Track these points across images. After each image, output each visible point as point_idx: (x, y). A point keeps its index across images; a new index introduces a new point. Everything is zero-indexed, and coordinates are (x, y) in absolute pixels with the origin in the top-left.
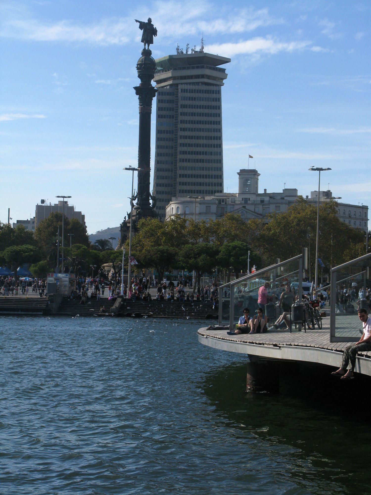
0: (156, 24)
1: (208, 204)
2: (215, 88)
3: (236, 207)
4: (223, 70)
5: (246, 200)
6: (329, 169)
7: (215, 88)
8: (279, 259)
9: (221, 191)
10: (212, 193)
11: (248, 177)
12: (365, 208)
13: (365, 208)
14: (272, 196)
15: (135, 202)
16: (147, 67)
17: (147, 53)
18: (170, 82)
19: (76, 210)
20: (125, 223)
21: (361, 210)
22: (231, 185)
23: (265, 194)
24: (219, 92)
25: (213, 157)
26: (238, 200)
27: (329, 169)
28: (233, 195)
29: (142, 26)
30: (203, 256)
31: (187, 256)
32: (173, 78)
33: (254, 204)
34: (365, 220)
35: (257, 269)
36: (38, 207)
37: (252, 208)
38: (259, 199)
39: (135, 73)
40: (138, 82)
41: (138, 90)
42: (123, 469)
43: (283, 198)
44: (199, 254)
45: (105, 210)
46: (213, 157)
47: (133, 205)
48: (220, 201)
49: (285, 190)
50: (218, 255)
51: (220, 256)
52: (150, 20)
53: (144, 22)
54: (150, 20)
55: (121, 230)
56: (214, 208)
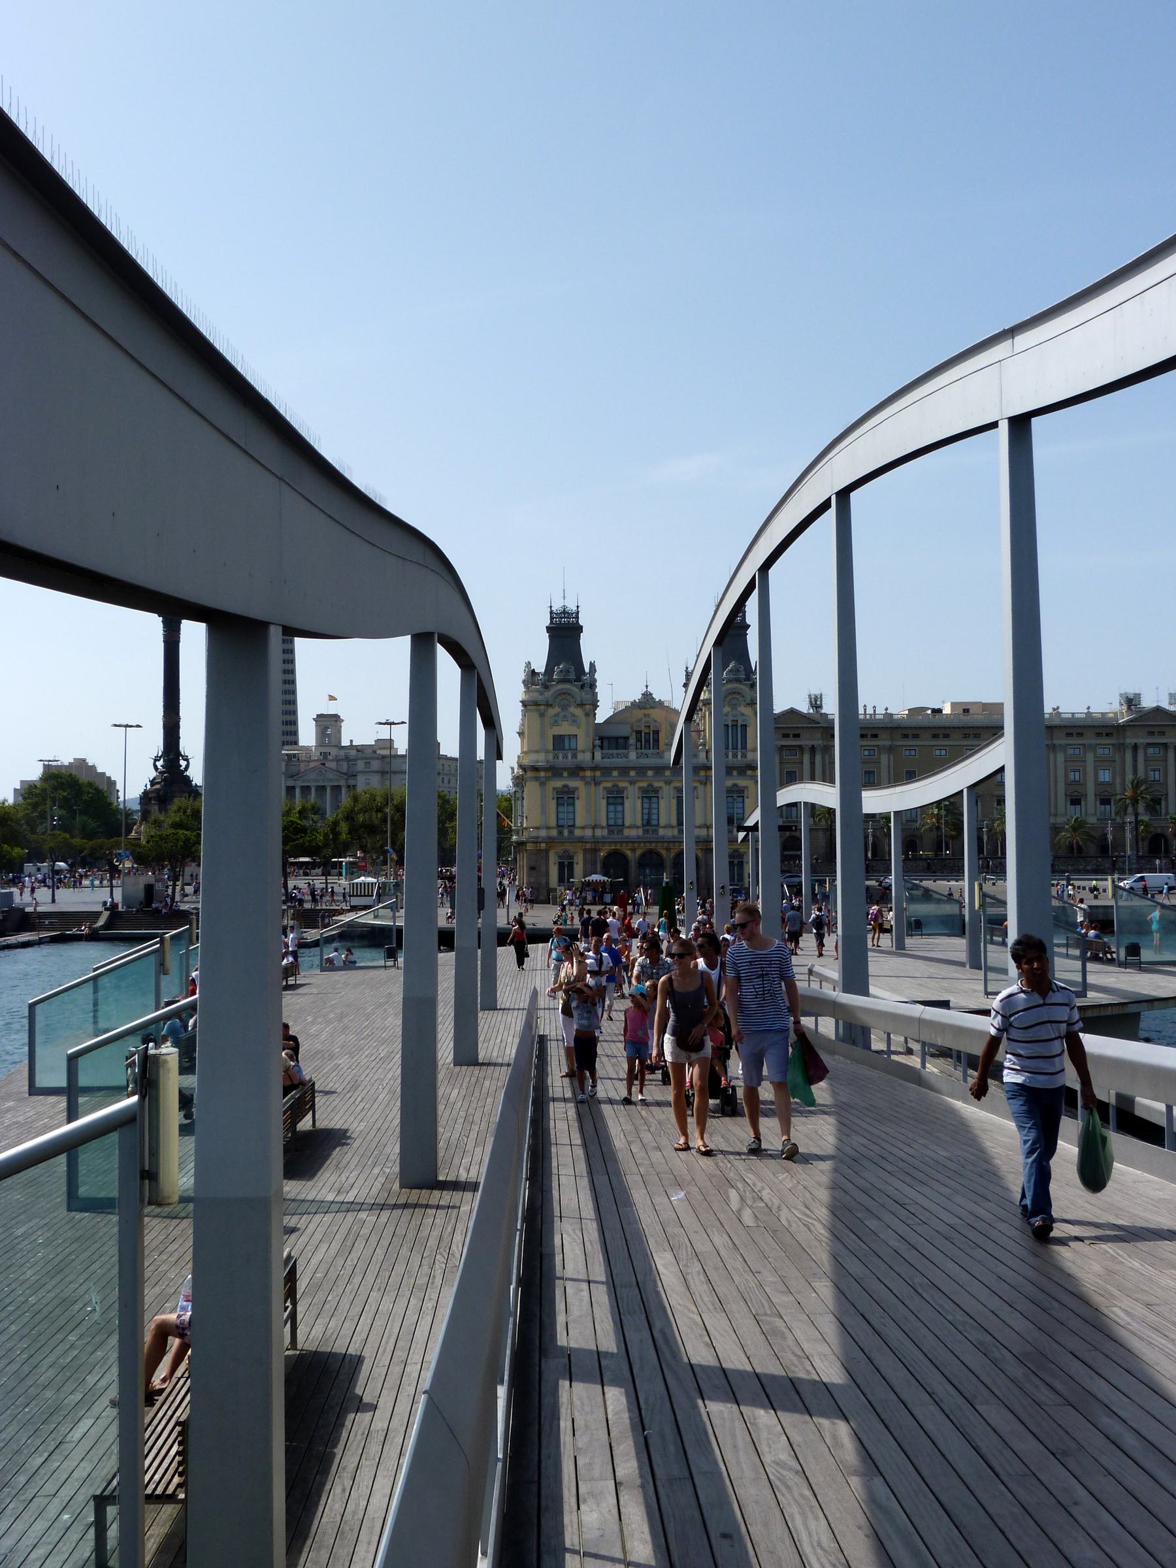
3: (312, 765)
5: (325, 755)
6: (138, 726)
8: (120, 909)
9: (296, 743)
11: (328, 724)
14: (360, 749)
15: (160, 764)
19: (99, 771)
20: (146, 793)
22: (307, 736)
23: (352, 746)
26: (315, 755)
27: (138, 726)
28: (307, 748)
33: (337, 760)
37: (333, 765)
38: (342, 753)
42: (735, 785)
43: (375, 752)
47: (156, 768)
48: (290, 757)
49: (378, 741)
55: (141, 803)
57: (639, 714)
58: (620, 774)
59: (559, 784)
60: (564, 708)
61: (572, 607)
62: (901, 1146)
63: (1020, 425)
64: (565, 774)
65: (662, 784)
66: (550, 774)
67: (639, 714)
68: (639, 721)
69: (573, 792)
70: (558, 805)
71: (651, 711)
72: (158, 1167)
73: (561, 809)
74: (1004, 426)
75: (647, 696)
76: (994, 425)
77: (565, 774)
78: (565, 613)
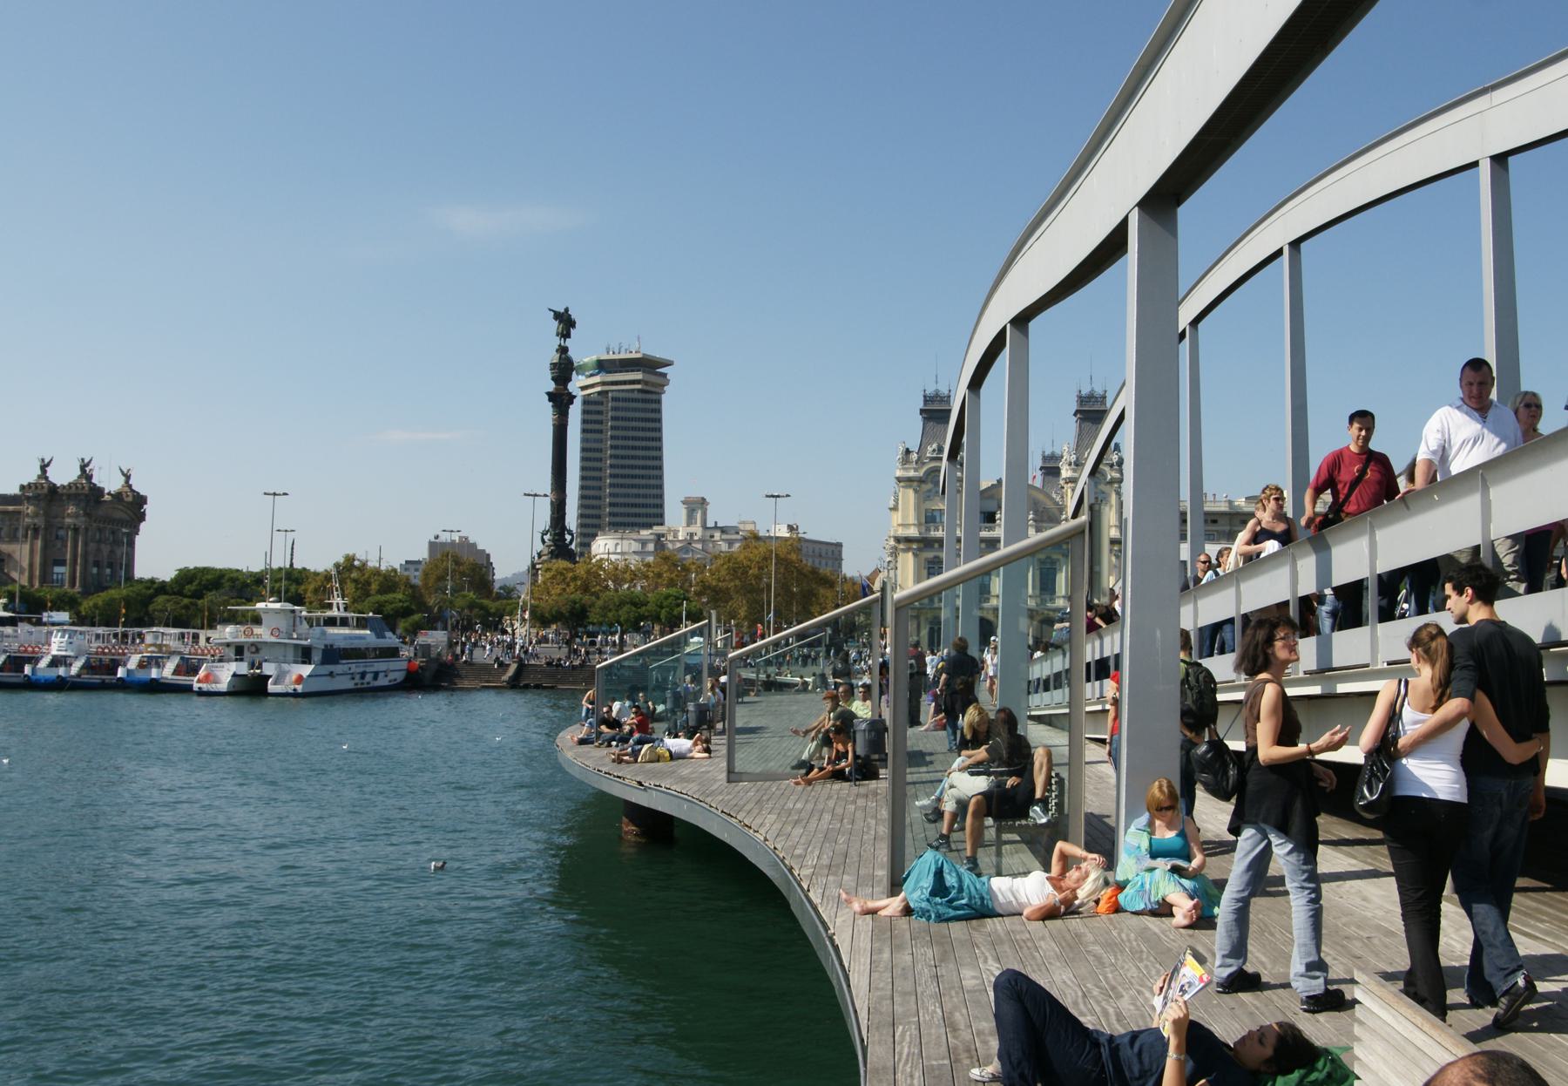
0: (574, 314)
1: (644, 543)
2: (654, 397)
4: (665, 375)
7: (654, 397)
10: (649, 526)
11: (695, 506)
12: (839, 545)
13: (839, 545)
15: (547, 538)
16: (563, 369)
17: (563, 350)
18: (598, 389)
21: (831, 548)
24: (659, 402)
25: (652, 482)
29: (558, 316)
30: (626, 608)
31: (605, 608)
32: (603, 384)
34: (838, 558)
35: (176, 672)
36: (431, 544)
39: (548, 375)
40: (551, 386)
41: (552, 396)
44: (622, 604)
45: (513, 552)
46: (652, 482)
50: (1454, 588)
51: (649, 607)
52: (567, 310)
53: (1400, 888)
54: (567, 310)
56: (651, 547)
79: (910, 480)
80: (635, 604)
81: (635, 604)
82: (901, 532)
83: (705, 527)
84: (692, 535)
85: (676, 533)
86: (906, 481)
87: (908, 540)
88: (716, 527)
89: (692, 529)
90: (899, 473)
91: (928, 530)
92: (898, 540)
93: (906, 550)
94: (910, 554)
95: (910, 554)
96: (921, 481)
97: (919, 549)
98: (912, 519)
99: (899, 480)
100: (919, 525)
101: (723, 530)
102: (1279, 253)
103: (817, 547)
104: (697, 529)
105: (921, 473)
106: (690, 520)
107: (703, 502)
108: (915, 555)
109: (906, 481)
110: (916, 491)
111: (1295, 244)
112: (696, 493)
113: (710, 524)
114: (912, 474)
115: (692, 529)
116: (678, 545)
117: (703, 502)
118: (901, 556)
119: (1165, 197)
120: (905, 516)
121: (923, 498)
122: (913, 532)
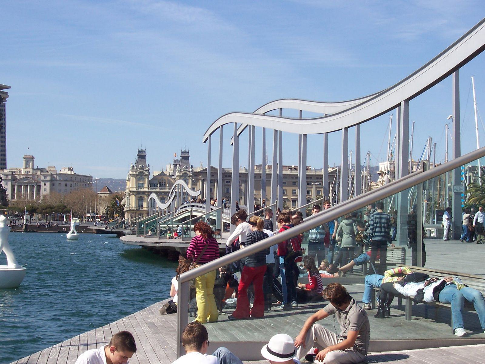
4: (6, 93)
57: (160, 177)
58: (164, 194)
59: (139, 196)
60: (141, 176)
61: (187, 151)
62: (51, 337)
63: (346, 129)
64: (141, 193)
65: (166, 196)
66: (137, 193)
67: (160, 177)
68: (160, 179)
69: (165, 198)
70: (139, 201)
71: (164, 177)
72: (418, 213)
73: (140, 202)
74: (343, 130)
75: (162, 173)
76: (341, 129)
77: (141, 193)
78: (185, 152)
79: (134, 175)
80: (51, 208)
81: (51, 208)
82: (131, 189)
83: (34, 169)
84: (27, 172)
85: (20, 171)
86: (133, 175)
87: (133, 192)
88: (38, 169)
89: (27, 170)
90: (131, 173)
91: (139, 189)
92: (130, 191)
93: (133, 194)
94: (134, 195)
95: (134, 195)
96: (137, 175)
97: (136, 194)
98: (134, 186)
99: (131, 175)
100: (136, 188)
101: (41, 170)
102: (219, 127)
103: (82, 178)
104: (30, 170)
105: (137, 173)
106: (27, 166)
107: (32, 158)
108: (135, 196)
109: (133, 175)
110: (135, 178)
111: (222, 126)
112: (29, 154)
113: (35, 167)
114: (134, 173)
115: (27, 170)
116: (22, 177)
117: (32, 158)
118: (131, 196)
119: (173, 200)
120: (132, 185)
121: (138, 180)
122: (135, 189)
